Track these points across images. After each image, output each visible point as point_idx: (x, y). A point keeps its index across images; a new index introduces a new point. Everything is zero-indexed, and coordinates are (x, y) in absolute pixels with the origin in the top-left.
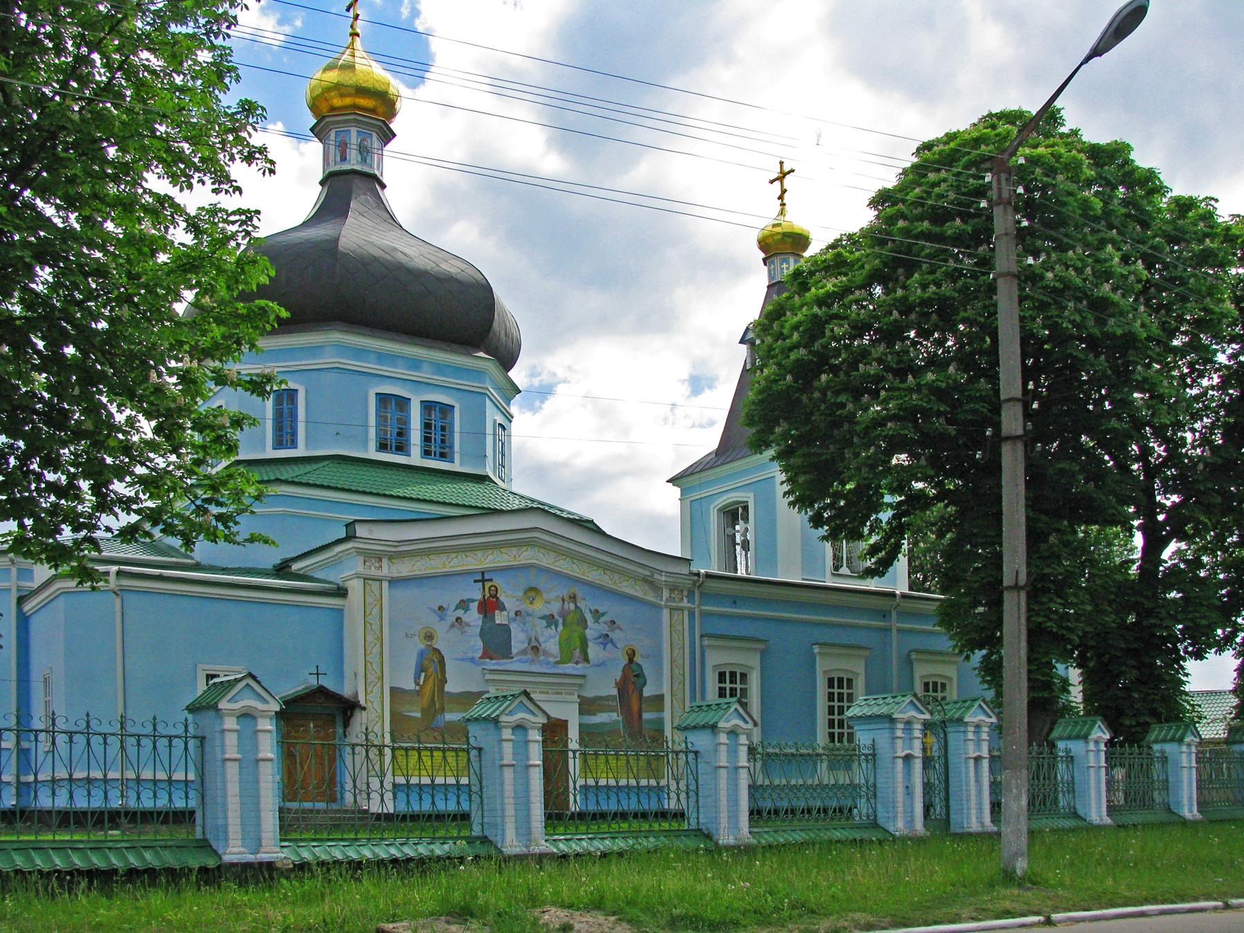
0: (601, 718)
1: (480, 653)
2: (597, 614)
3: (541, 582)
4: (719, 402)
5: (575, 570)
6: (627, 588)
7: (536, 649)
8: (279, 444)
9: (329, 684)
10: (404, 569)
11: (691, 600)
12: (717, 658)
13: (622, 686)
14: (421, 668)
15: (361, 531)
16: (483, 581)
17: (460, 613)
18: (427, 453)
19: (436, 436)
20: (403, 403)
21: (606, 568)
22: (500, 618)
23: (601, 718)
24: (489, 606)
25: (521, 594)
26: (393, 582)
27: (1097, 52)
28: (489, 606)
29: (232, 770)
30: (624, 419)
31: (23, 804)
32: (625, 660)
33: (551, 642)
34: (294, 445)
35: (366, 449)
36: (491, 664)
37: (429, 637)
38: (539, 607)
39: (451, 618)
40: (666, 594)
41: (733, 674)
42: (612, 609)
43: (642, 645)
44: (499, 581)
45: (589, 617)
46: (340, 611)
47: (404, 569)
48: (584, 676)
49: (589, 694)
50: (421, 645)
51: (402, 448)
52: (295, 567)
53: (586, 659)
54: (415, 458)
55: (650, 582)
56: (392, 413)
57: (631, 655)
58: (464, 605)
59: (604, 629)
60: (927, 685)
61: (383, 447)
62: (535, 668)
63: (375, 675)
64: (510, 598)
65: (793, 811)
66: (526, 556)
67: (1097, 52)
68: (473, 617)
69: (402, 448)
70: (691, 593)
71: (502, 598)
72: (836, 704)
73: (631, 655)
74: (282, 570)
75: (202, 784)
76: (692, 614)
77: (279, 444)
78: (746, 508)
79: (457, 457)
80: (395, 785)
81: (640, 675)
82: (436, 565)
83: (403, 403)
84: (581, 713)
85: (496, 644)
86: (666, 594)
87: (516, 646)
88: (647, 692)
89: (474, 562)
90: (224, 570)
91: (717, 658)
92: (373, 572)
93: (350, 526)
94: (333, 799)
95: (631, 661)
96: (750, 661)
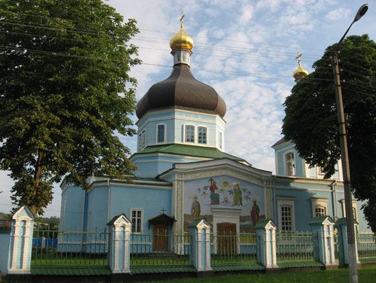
0: (247, 223)
1: (210, 203)
2: (244, 190)
3: (229, 181)
4: (279, 126)
5: (238, 176)
6: (253, 181)
7: (227, 201)
8: (159, 141)
9: (166, 213)
10: (189, 177)
11: (272, 184)
12: (280, 203)
13: (252, 212)
14: (193, 208)
15: (177, 166)
16: (211, 180)
17: (204, 190)
18: (200, 142)
19: (202, 136)
20: (193, 128)
21: (247, 175)
22: (216, 192)
23: (247, 223)
24: (213, 188)
25: (222, 184)
26: (185, 181)
27: (356, 20)
28: (213, 188)
29: (200, 244)
30: (250, 129)
31: (84, 251)
32: (253, 205)
33: (231, 199)
34: (163, 141)
35: (155, 142)
36: (214, 206)
37: (196, 198)
38: (227, 188)
39: (202, 192)
40: (265, 183)
41: (286, 208)
42: (249, 188)
43: (258, 199)
44: (216, 180)
45: (242, 191)
46: (171, 191)
47: (189, 177)
48: (240, 210)
49: (242, 215)
50: (193, 201)
51: (192, 141)
52: (161, 177)
53: (241, 204)
54: (196, 143)
55: (260, 179)
56: (190, 130)
57: (255, 202)
58: (205, 188)
59: (246, 194)
60: (283, 208)
61: (188, 140)
62: (226, 207)
63: (181, 211)
64: (219, 185)
65: (283, 246)
66: (224, 172)
67: (356, 20)
68: (208, 192)
69: (192, 141)
70: (272, 182)
71: (217, 185)
72: (285, 216)
73: (255, 202)
74: (157, 178)
75: (192, 247)
76: (273, 189)
77: (159, 141)
78: (293, 155)
79: (208, 142)
80: (185, 246)
81: (258, 209)
82: (198, 176)
83: (193, 128)
84: (240, 221)
85: (215, 200)
86: (265, 183)
87: (221, 201)
88: (260, 214)
89: (208, 175)
90: (142, 179)
91: (280, 203)
92: (180, 179)
93: (174, 165)
94: (167, 250)
95: (255, 205)
96: (292, 203)
